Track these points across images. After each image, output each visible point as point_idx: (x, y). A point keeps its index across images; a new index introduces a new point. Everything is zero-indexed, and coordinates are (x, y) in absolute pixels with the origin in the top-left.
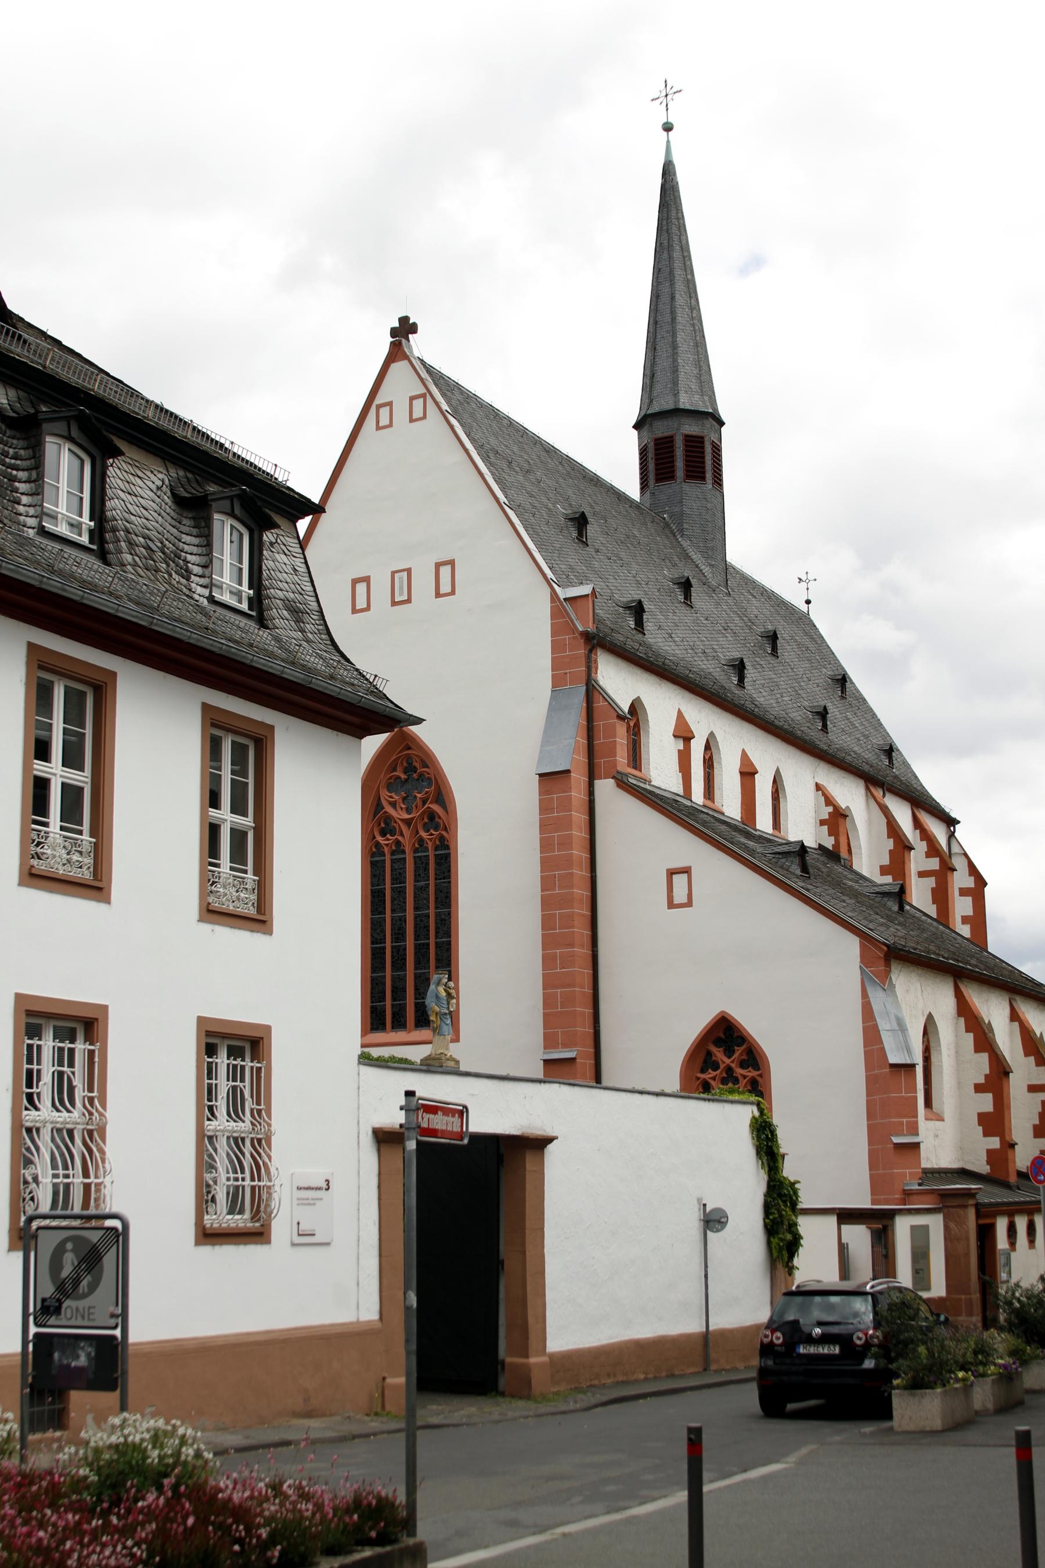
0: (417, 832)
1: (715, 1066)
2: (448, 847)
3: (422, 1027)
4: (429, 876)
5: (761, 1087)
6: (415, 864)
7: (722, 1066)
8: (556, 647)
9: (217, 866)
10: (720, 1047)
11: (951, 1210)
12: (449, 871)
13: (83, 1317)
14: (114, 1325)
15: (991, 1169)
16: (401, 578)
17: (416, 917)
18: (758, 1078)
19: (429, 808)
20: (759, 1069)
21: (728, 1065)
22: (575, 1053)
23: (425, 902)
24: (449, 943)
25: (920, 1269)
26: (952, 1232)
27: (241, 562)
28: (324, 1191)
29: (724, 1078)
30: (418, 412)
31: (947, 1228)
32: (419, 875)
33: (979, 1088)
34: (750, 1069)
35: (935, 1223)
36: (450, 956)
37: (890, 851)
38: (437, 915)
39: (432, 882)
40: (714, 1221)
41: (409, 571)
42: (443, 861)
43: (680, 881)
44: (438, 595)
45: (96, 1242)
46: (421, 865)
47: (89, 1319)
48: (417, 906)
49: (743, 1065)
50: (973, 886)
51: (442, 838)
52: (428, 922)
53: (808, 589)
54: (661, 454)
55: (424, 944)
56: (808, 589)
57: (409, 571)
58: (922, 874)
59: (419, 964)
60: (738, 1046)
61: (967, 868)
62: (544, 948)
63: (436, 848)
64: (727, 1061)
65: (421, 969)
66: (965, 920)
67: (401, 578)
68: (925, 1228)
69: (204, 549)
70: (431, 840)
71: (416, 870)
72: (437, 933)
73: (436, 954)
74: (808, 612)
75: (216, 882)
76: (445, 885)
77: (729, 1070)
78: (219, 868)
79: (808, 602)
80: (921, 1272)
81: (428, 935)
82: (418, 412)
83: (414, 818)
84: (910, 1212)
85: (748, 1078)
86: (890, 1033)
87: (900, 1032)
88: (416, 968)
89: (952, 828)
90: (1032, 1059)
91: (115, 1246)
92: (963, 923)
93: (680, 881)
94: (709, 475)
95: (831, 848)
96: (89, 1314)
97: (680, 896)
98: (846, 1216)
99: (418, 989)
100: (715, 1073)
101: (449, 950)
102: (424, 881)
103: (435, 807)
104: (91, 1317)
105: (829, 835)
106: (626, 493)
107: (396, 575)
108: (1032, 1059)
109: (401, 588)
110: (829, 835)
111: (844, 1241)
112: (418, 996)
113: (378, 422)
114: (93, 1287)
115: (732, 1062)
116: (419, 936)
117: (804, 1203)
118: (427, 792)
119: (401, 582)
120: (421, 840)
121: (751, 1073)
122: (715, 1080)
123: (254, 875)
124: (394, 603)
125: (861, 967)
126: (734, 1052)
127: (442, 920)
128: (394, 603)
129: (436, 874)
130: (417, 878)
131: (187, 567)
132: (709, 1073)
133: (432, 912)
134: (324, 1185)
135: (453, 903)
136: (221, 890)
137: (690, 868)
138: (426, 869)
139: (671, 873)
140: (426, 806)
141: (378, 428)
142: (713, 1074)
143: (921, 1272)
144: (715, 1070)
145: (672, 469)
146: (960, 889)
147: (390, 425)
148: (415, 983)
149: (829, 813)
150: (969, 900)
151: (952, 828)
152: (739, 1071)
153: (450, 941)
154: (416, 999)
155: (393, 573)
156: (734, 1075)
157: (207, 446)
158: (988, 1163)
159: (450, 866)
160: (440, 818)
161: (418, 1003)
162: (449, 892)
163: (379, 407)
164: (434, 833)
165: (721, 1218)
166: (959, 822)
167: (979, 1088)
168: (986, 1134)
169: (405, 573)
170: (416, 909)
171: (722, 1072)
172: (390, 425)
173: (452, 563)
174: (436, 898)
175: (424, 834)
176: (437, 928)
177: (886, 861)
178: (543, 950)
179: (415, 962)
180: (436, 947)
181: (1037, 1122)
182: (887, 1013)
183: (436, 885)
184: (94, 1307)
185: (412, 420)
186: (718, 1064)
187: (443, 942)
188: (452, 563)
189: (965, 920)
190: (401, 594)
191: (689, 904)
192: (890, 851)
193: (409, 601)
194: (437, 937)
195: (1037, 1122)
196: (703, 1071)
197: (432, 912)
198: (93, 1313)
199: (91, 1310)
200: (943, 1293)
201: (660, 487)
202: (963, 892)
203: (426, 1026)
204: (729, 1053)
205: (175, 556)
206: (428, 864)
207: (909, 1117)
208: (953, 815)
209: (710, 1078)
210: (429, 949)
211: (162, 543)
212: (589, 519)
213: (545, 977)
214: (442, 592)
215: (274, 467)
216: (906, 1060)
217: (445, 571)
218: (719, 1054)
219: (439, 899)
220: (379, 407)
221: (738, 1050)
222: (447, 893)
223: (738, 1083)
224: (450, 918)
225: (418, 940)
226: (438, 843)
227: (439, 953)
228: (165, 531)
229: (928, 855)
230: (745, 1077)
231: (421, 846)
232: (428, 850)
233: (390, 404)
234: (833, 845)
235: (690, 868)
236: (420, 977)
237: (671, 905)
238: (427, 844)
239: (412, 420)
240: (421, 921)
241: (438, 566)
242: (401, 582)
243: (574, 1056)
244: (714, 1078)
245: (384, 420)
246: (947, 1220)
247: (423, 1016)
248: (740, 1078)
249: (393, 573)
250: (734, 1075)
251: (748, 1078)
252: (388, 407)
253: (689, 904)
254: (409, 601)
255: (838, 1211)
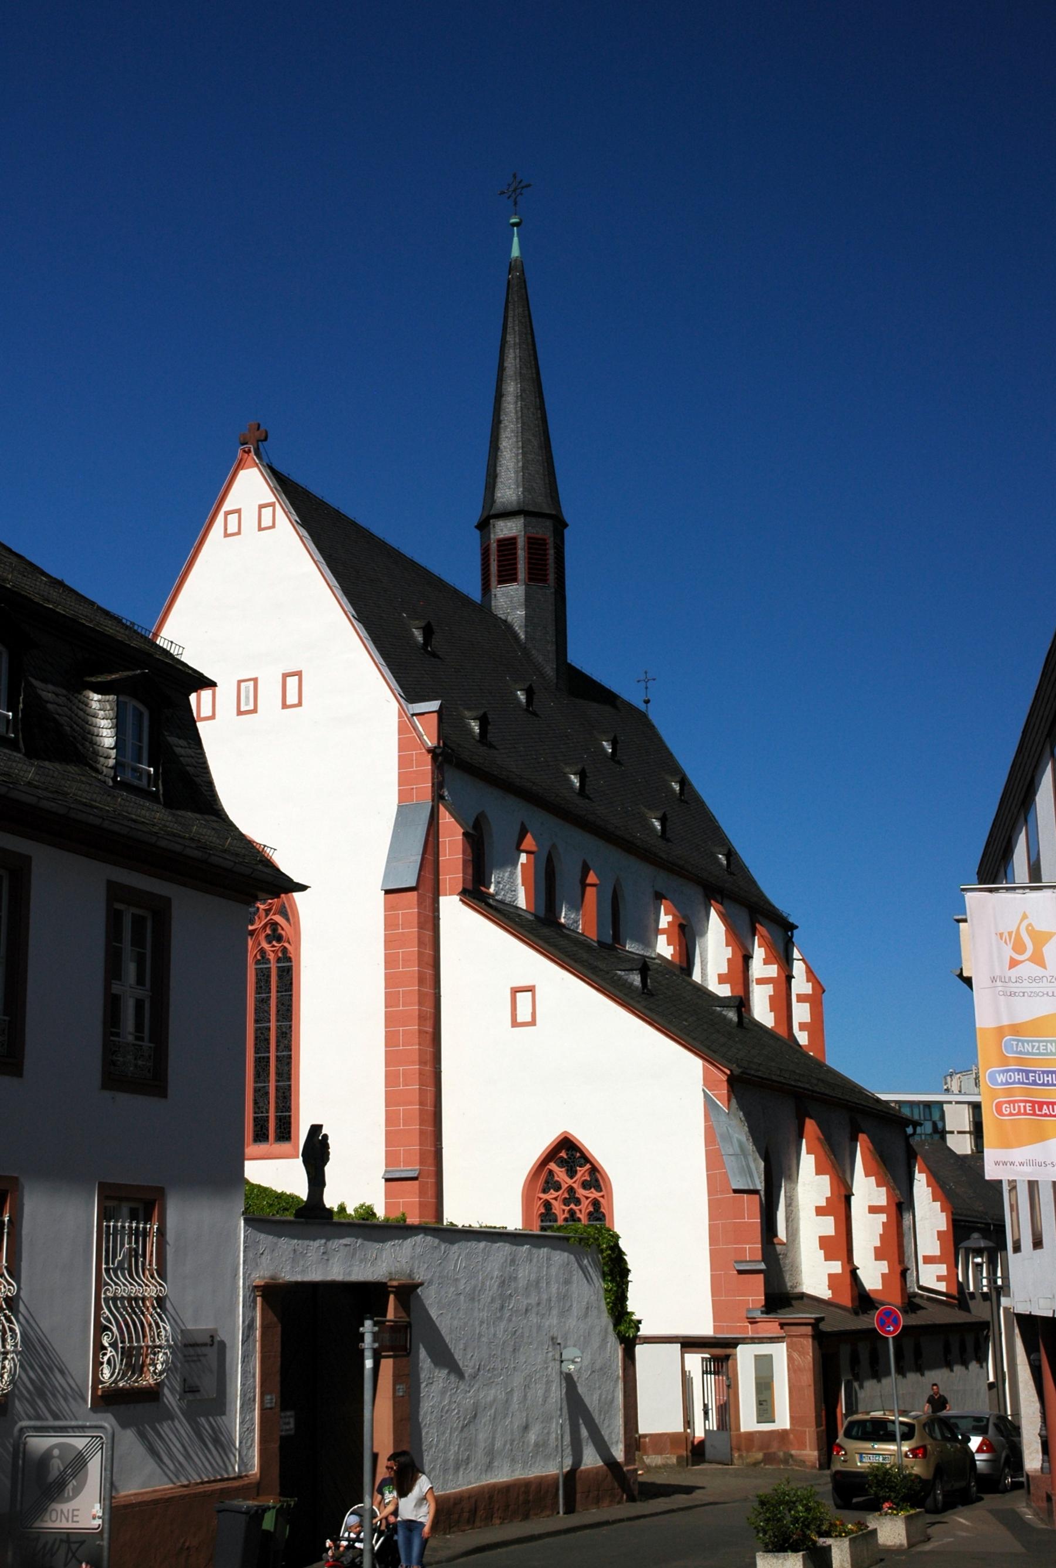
0: (259, 944)
1: (557, 1187)
2: (289, 960)
3: (260, 1141)
4: (270, 989)
5: (604, 1209)
6: (257, 975)
7: (564, 1186)
8: (403, 762)
9: (118, 1035)
10: (562, 1167)
11: (795, 1339)
12: (291, 984)
13: (67, 1520)
14: (97, 1526)
15: (833, 1294)
16: (247, 688)
17: (257, 1030)
18: (601, 1199)
19: (271, 919)
20: (601, 1191)
21: (570, 1186)
22: (417, 1172)
23: (266, 1014)
24: (290, 1057)
25: (764, 1401)
26: (796, 1363)
27: (140, 740)
28: (209, 1348)
29: (565, 1198)
30: (267, 521)
31: (790, 1358)
32: (261, 987)
33: (820, 1211)
34: (592, 1190)
35: (779, 1352)
36: (290, 1070)
37: (729, 960)
38: (278, 1028)
39: (274, 994)
40: (568, 1360)
41: (255, 680)
42: (285, 974)
43: (523, 998)
44: (285, 706)
45: (81, 1449)
46: (263, 978)
47: (73, 1521)
48: (258, 1018)
49: (585, 1185)
50: (810, 992)
51: (285, 950)
52: (269, 1035)
53: (647, 688)
54: (505, 566)
55: (264, 1058)
56: (647, 688)
57: (255, 680)
58: (761, 981)
59: (259, 1077)
60: (580, 1167)
61: (805, 974)
62: (387, 1065)
63: (279, 960)
64: (570, 1182)
65: (260, 1082)
66: (803, 1027)
67: (247, 688)
68: (769, 1358)
69: (109, 731)
70: (273, 951)
71: (258, 982)
72: (277, 1046)
73: (277, 1067)
74: (647, 711)
75: (116, 1051)
76: (287, 997)
77: (571, 1189)
78: (119, 1037)
79: (647, 702)
80: (764, 1403)
81: (269, 1048)
82: (267, 521)
83: (256, 929)
84: (753, 1341)
85: (590, 1200)
86: (733, 1158)
87: (742, 1157)
88: (256, 1082)
89: (789, 933)
90: (873, 1179)
91: (100, 1451)
92: (801, 1030)
93: (523, 998)
94: (551, 577)
95: (669, 958)
96: (73, 1516)
97: (524, 1015)
98: (689, 1344)
99: (257, 1103)
100: (557, 1194)
101: (289, 1064)
102: (265, 993)
103: (278, 918)
104: (75, 1519)
105: (668, 945)
106: (470, 596)
107: (243, 684)
108: (873, 1179)
109: (247, 698)
110: (668, 945)
111: (687, 1369)
112: (257, 1110)
113: (226, 529)
114: (77, 1491)
115: (575, 1182)
116: (259, 1049)
117: (644, 1331)
118: (271, 904)
119: (247, 692)
120: (262, 951)
121: (593, 1194)
122: (556, 1200)
123: (150, 1041)
124: (240, 713)
125: (703, 1090)
126: (576, 1172)
127: (283, 1033)
128: (240, 713)
129: (278, 987)
130: (259, 990)
131: (94, 749)
132: (552, 1194)
133: (273, 1025)
134: (208, 1341)
135: (294, 1017)
136: (121, 1059)
137: (534, 987)
138: (268, 981)
139: (515, 991)
140: (269, 918)
141: (226, 535)
142: (555, 1194)
143: (764, 1403)
144: (557, 1191)
145: (514, 577)
146: (798, 995)
147: (239, 533)
148: (255, 1097)
149: (668, 922)
150: (806, 1006)
151: (789, 933)
152: (581, 1192)
153: (291, 1055)
154: (255, 1113)
155: (240, 682)
156: (577, 1195)
157: (110, 629)
158: (830, 1288)
159: (292, 979)
160: (283, 929)
161: (257, 1118)
162: (290, 1006)
163: (227, 513)
164: (276, 944)
165: (575, 1358)
166: (797, 927)
167: (820, 1211)
168: (828, 1258)
169: (252, 683)
170: (256, 1021)
171: (563, 1193)
172: (239, 533)
173: (299, 674)
174: (278, 1011)
175: (265, 946)
176: (278, 1042)
177: (724, 970)
178: (386, 1066)
179: (254, 1075)
180: (277, 1061)
181: (878, 1244)
182: (731, 1137)
183: (277, 998)
184: (78, 1510)
185: (260, 529)
186: (560, 1185)
187: (284, 1056)
188: (299, 674)
189: (803, 1027)
190: (247, 704)
191: (533, 1023)
192: (729, 960)
193: (255, 711)
194: (277, 1050)
195: (878, 1244)
196: (544, 1191)
197: (273, 1025)
198: (77, 1516)
199: (76, 1513)
200: (788, 1426)
201: (502, 589)
202: (801, 998)
203: (264, 1141)
204: (572, 1173)
205: (83, 739)
206: (269, 976)
207: (753, 1244)
208: (791, 920)
209: (553, 1199)
210: (268, 1062)
211: (71, 727)
212: (434, 627)
213: (388, 1094)
214: (288, 703)
215: (170, 643)
216: (749, 1186)
217: (292, 682)
218: (560, 1174)
219: (280, 1013)
220: (227, 513)
221: (580, 1171)
222: (288, 1006)
223: (580, 1204)
224: (291, 1031)
225: (258, 1053)
226: (280, 955)
227: (279, 1066)
228: (73, 715)
229: (766, 962)
230: (587, 1198)
231: (263, 957)
232: (270, 962)
233: (238, 511)
234: (672, 955)
235: (534, 987)
236: (259, 1090)
237: (515, 1023)
238: (269, 955)
239: (260, 529)
240: (262, 1033)
241: (285, 676)
242: (247, 692)
243: (416, 1175)
244: (556, 1199)
245: (232, 528)
246: (790, 1350)
247: (261, 1131)
248: (583, 1199)
249: (240, 682)
250: (577, 1195)
251: (590, 1200)
252: (237, 515)
253: (533, 1023)
254: (255, 711)
255: (681, 1340)
